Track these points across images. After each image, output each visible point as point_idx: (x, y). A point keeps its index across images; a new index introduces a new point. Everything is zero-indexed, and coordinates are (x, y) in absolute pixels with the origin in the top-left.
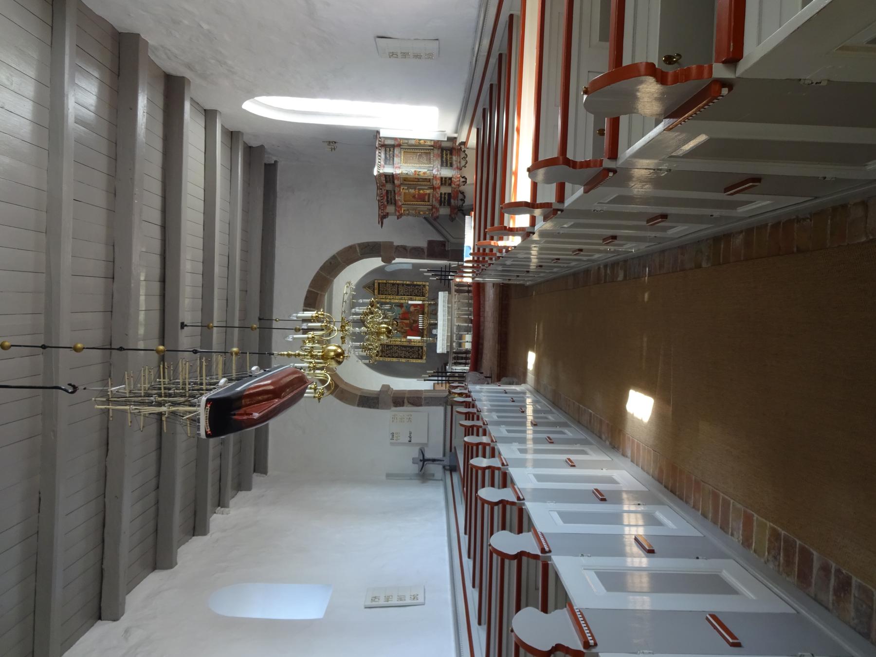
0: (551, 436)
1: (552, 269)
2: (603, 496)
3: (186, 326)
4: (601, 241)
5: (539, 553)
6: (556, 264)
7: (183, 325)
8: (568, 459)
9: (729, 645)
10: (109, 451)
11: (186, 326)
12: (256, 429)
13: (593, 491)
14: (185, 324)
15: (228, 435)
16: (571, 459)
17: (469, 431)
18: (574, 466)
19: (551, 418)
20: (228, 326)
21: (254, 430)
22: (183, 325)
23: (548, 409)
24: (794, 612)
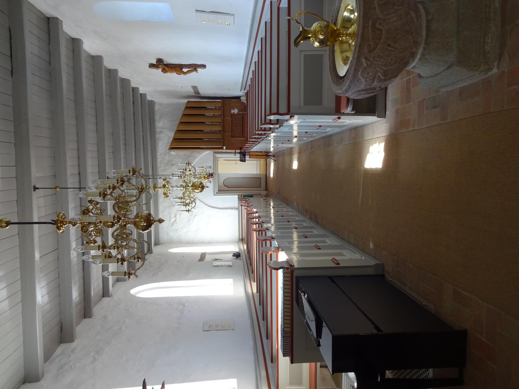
0: (318, 244)
1: (326, 129)
2: (319, 247)
3: (38, 188)
4: (332, 121)
5: (289, 267)
6: (305, 135)
7: (35, 188)
8: (333, 258)
9: (335, 264)
10: (257, 156)
11: (38, 188)
12: (147, 232)
13: (332, 259)
14: (36, 187)
15: (37, 305)
16: (336, 259)
17: (250, 211)
18: (320, 249)
19: (315, 232)
20: (81, 187)
21: (146, 233)
22: (35, 188)
23: (295, 214)
24: (324, 234)
